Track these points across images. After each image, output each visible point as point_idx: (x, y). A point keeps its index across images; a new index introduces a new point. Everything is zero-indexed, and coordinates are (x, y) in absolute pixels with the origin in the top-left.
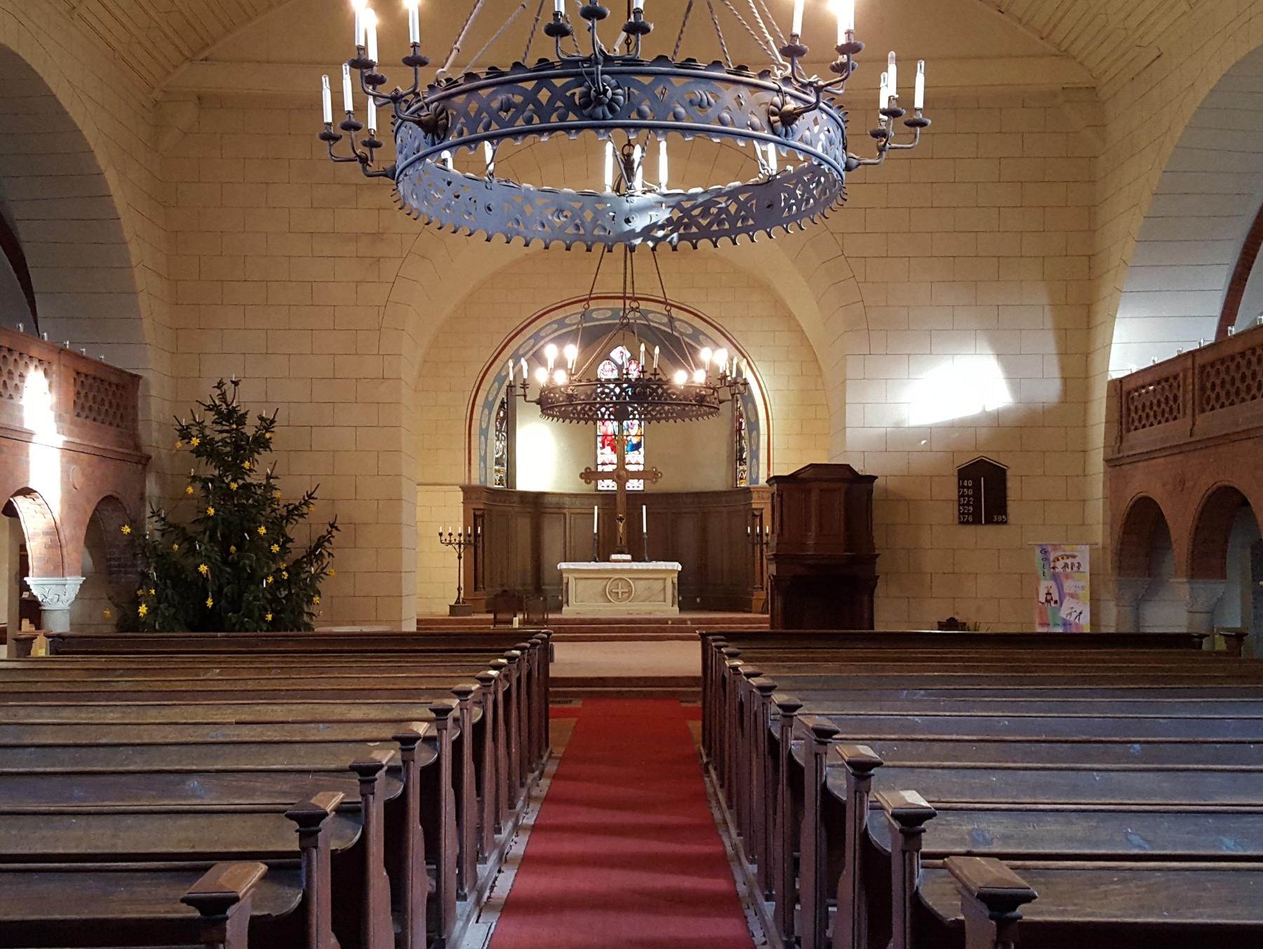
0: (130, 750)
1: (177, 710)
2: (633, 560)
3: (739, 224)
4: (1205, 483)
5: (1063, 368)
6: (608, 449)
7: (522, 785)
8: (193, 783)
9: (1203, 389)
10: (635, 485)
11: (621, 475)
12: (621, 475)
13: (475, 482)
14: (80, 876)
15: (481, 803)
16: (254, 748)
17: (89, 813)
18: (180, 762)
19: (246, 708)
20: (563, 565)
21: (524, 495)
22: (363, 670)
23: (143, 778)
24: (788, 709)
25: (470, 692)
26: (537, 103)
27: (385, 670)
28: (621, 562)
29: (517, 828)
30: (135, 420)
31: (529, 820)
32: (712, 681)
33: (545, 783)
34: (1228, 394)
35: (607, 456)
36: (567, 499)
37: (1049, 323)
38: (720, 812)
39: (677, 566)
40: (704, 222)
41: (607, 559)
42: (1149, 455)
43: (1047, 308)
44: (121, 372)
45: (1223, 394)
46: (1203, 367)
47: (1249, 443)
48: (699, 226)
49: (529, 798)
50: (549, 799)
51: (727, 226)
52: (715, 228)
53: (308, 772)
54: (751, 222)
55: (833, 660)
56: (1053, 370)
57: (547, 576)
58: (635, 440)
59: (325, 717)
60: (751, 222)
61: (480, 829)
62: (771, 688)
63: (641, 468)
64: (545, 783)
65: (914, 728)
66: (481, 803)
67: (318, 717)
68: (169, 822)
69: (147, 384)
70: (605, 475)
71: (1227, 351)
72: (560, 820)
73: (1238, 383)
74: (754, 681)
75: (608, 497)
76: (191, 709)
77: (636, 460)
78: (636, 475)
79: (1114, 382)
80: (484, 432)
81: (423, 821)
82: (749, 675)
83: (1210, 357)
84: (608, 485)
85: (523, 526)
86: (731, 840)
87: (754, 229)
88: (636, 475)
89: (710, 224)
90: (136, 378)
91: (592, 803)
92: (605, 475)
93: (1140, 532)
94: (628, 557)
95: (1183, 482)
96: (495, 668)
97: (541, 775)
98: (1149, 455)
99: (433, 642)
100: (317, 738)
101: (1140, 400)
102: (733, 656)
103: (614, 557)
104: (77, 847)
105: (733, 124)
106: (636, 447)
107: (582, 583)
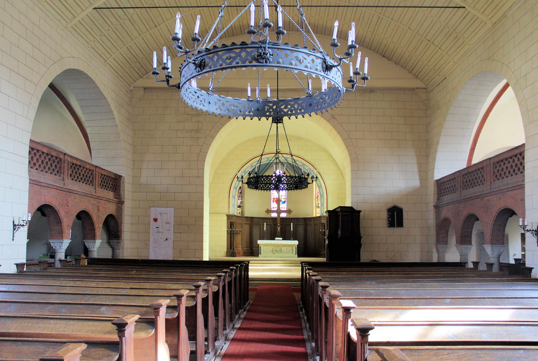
0: (89, 296)
1: (114, 283)
2: (283, 240)
3: (299, 111)
4: (465, 213)
5: (420, 176)
6: (275, 203)
7: (237, 313)
8: (103, 309)
9: (463, 182)
10: (283, 215)
11: (279, 211)
12: (279, 211)
13: (231, 213)
14: (26, 343)
15: (217, 320)
16: (131, 297)
17: (57, 319)
18: (105, 301)
19: (137, 284)
20: (260, 242)
21: (247, 217)
22: (182, 272)
23: (85, 306)
24: (324, 287)
25: (211, 280)
26: (273, 109)
27: (190, 272)
28: (279, 241)
29: (233, 328)
30: (119, 190)
31: (238, 326)
32: (303, 279)
33: (245, 313)
34: (471, 184)
35: (274, 206)
36: (261, 220)
37: (415, 161)
38: (305, 325)
39: (296, 242)
40: (286, 110)
41: (274, 239)
42: (448, 204)
43: (414, 157)
44: (116, 175)
45: (470, 184)
46: (463, 176)
47: (479, 199)
48: (284, 112)
49: (239, 318)
50: (245, 319)
51: (294, 112)
52: (289, 112)
53: (144, 306)
54: (303, 111)
55: (345, 271)
56: (417, 177)
57: (254, 245)
58: (283, 200)
59: (163, 288)
60: (303, 111)
61: (216, 329)
62: (320, 280)
63: (286, 209)
64: (245, 313)
65: (371, 294)
66: (217, 320)
67: (161, 288)
68: (85, 323)
69: (124, 178)
70: (274, 212)
71: (470, 170)
72: (249, 326)
73: (474, 181)
74: (313, 278)
75: (274, 219)
76: (119, 283)
77: (283, 207)
78: (284, 212)
79: (437, 181)
80: (234, 197)
81: (187, 325)
82: (313, 276)
83: (465, 172)
84: (274, 215)
85: (246, 228)
86: (306, 335)
87: (304, 113)
88: (284, 212)
89: (288, 111)
90: (121, 176)
91: (257, 320)
92: (274, 212)
93: (442, 227)
94: (281, 239)
95: (458, 213)
96: (224, 272)
97: (244, 311)
98: (448, 204)
99: (214, 265)
100: (152, 295)
101: (443, 185)
102: (309, 269)
103: (276, 238)
104: (51, 331)
105: (283, 63)
106: (284, 202)
107: (265, 247)
